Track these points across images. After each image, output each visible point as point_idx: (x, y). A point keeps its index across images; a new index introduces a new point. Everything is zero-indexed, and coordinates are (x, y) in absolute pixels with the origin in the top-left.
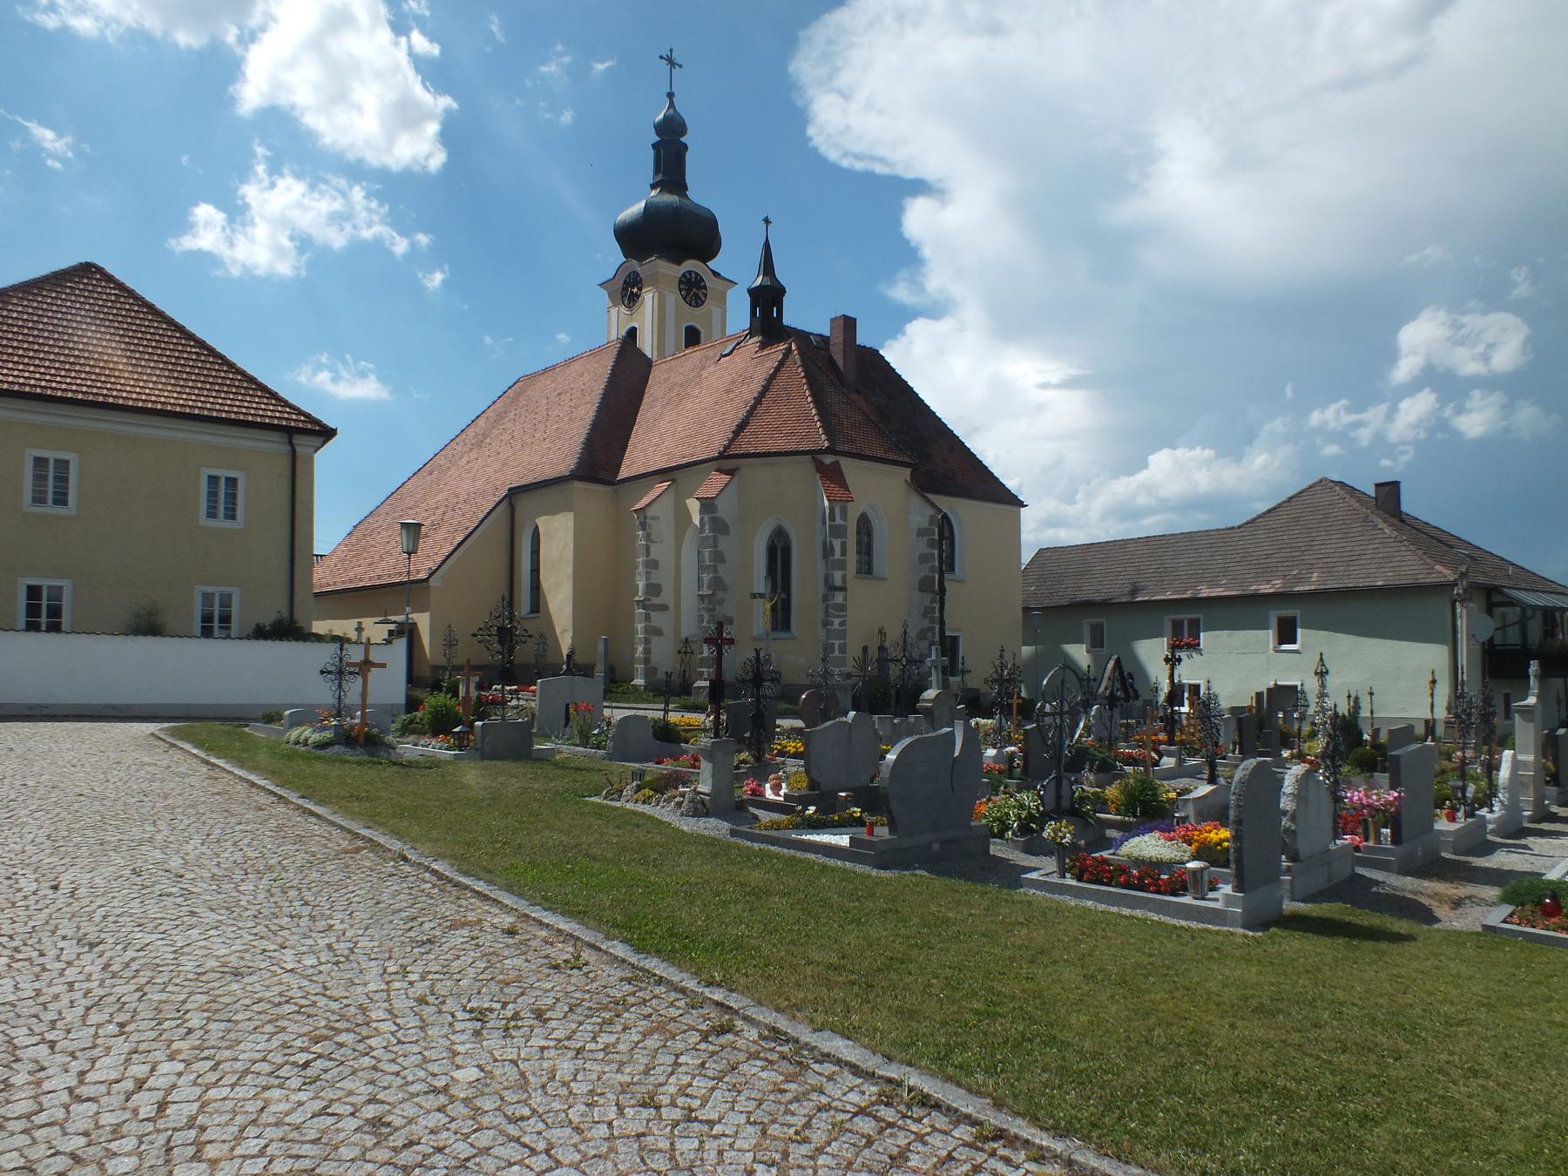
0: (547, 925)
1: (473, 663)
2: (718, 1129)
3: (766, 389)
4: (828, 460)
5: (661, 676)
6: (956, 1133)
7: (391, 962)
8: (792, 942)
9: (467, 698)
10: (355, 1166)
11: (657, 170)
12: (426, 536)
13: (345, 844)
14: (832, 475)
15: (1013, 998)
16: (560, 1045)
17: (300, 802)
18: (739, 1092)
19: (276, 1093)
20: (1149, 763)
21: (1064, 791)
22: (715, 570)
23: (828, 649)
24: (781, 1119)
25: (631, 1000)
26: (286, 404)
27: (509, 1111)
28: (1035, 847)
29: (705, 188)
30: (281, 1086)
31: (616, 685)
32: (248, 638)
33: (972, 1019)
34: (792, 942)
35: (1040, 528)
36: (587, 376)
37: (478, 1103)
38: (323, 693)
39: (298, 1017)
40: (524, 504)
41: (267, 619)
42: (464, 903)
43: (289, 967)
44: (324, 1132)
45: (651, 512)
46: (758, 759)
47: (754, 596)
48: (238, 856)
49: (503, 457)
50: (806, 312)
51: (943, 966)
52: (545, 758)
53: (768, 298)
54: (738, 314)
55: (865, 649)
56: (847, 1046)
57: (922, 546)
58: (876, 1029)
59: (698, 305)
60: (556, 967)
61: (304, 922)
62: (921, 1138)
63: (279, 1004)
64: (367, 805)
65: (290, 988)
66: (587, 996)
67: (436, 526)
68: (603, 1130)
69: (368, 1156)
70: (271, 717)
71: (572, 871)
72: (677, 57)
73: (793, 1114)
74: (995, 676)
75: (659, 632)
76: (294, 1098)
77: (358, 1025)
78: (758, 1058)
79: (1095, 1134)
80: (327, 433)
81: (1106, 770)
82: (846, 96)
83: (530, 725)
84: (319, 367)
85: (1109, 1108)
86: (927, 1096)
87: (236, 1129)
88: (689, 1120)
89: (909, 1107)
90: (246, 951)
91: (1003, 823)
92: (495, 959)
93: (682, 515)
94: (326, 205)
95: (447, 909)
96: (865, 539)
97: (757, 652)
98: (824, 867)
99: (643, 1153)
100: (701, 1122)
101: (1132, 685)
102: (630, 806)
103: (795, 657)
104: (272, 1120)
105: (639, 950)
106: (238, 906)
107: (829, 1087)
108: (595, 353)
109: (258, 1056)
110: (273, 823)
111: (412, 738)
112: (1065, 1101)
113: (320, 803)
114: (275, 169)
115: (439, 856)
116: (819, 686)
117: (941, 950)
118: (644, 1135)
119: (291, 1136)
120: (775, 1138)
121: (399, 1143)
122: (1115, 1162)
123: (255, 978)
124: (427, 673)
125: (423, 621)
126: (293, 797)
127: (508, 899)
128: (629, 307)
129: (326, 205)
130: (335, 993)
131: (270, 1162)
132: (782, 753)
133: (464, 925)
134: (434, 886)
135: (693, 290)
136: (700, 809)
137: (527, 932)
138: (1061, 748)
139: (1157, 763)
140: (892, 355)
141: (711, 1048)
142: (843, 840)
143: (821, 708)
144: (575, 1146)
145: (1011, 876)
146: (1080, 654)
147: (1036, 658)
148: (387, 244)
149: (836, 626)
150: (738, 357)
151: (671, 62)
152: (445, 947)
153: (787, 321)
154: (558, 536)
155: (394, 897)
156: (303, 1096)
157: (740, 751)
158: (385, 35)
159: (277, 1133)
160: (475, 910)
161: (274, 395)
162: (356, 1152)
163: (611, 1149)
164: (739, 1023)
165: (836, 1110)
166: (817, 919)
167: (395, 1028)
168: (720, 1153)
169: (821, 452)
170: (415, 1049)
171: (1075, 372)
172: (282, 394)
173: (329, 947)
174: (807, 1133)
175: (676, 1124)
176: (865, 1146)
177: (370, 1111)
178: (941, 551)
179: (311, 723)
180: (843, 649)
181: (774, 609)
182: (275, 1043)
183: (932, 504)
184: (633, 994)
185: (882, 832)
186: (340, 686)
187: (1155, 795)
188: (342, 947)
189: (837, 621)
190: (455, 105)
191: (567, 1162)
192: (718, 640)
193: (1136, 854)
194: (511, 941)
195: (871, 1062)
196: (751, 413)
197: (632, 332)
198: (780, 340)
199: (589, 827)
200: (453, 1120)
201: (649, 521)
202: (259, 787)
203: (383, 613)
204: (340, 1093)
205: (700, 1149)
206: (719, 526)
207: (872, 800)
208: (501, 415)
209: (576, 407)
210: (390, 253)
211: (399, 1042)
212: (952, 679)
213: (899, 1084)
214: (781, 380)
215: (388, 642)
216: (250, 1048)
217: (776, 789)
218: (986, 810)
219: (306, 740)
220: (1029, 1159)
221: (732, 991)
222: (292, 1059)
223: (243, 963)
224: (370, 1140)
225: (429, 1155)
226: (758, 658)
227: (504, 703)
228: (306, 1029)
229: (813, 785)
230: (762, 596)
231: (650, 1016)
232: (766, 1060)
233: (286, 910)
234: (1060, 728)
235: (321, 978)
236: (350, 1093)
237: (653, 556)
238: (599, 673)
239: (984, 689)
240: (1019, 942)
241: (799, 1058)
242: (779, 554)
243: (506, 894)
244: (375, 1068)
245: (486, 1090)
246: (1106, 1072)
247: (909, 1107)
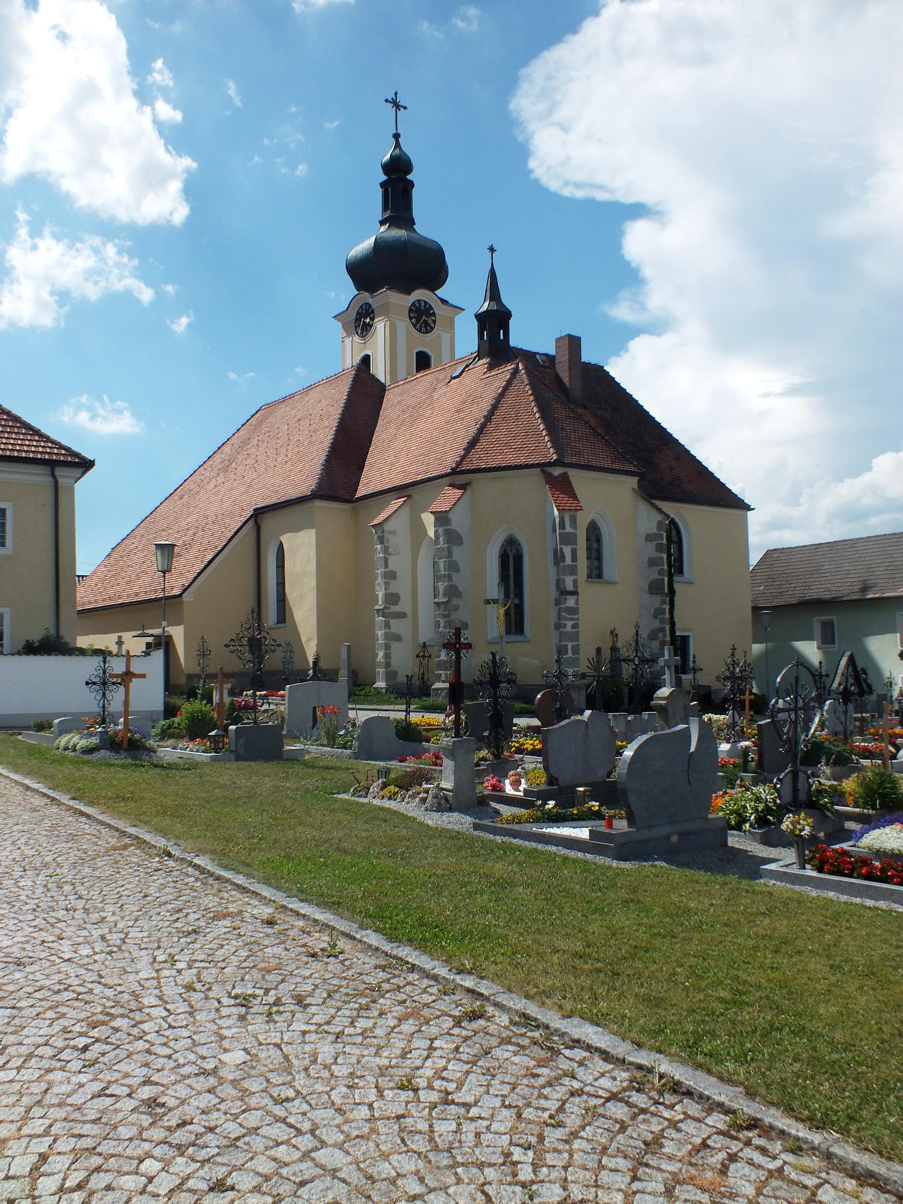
0: (304, 916)
1: (226, 670)
2: (474, 1112)
3: (495, 407)
4: (557, 471)
5: (401, 678)
6: (710, 1121)
7: (161, 951)
8: (538, 931)
9: (221, 703)
10: (133, 1145)
11: (385, 208)
12: (179, 555)
13: (113, 841)
14: (562, 486)
15: (759, 987)
16: (320, 1029)
17: (71, 803)
18: (493, 1076)
19: (58, 1076)
20: (887, 756)
21: (801, 785)
22: (450, 578)
23: (561, 650)
24: (535, 1103)
25: (386, 986)
26: (48, 439)
27: (275, 1092)
28: (773, 838)
29: (429, 221)
30: (62, 1069)
31: (359, 688)
32: (19, 653)
33: (719, 1008)
34: (538, 931)
35: (764, 533)
36: (324, 403)
37: (246, 1084)
38: (89, 702)
39: (76, 1004)
40: (269, 523)
41: (36, 636)
42: (225, 895)
43: (66, 956)
44: (103, 1112)
45: (388, 527)
46: (497, 756)
47: (488, 602)
48: (17, 854)
49: (247, 480)
50: (530, 334)
51: (686, 955)
52: (295, 758)
53: (494, 322)
54: (466, 337)
55: (599, 650)
56: (596, 1033)
57: (650, 550)
58: (624, 1016)
59: (427, 332)
60: (314, 955)
61: (79, 914)
62: (674, 1125)
63: (59, 991)
64: (132, 804)
65: (68, 976)
66: (344, 983)
67: (187, 546)
68: (364, 1112)
69: (145, 1135)
70: (42, 726)
71: (325, 864)
72: (402, 100)
73: (546, 1098)
74: (727, 674)
75: (398, 638)
76: (75, 1079)
77: (131, 1011)
78: (510, 1043)
79: (853, 1127)
80: (86, 465)
81: (843, 763)
82: (565, 128)
83: (280, 727)
84: (79, 408)
85: (865, 1101)
86: (678, 1083)
87: (23, 1109)
88: (447, 1102)
89: (661, 1093)
90: (27, 942)
91: (740, 815)
92: (255, 948)
93: (418, 528)
94: (84, 262)
95: (210, 901)
96: (595, 545)
97: (494, 655)
98: (565, 859)
99: (404, 1135)
100: (458, 1104)
101: (865, 680)
102: (376, 802)
103: (529, 659)
104: (55, 1101)
105: (391, 939)
106: (18, 900)
107: (580, 1072)
108: (331, 380)
109: (42, 1040)
110: (47, 823)
111: (171, 742)
112: (818, 1091)
113: (90, 803)
114: (36, 232)
115: (200, 852)
116: (554, 686)
117: (684, 939)
118: (403, 1116)
119: (72, 1117)
120: (530, 1122)
121: (173, 1123)
122: (876, 1157)
123: (35, 967)
124: (182, 681)
125: (177, 633)
126: (65, 799)
127: (266, 892)
128: (363, 336)
129: (84, 262)
130: (110, 981)
131: (55, 1141)
132: (520, 751)
133: (225, 916)
134: (197, 880)
135: (423, 318)
136: (444, 804)
137: (285, 922)
138: (797, 743)
139: (894, 757)
140: (617, 370)
141: (464, 1033)
142: (582, 833)
143: (555, 709)
144: (338, 1126)
145: (751, 867)
146: (810, 651)
147: (766, 654)
148: (135, 293)
149: (569, 628)
150: (467, 378)
151: (397, 105)
152: (209, 937)
153: (512, 343)
154: (301, 552)
155: (160, 890)
156: (83, 1078)
157: (479, 749)
158: (133, 103)
159: (60, 1113)
160: (236, 902)
161: (37, 432)
162: (133, 1131)
163: (373, 1130)
164: (490, 1010)
165: (589, 1095)
166: (561, 909)
167: (165, 1014)
168: (478, 1135)
169: (550, 464)
170: (185, 1033)
171: (797, 380)
172: (44, 431)
173: (103, 938)
174: (561, 1117)
175: (433, 1106)
176: (619, 1132)
177: (146, 1092)
178: (669, 556)
179: (78, 730)
180: (576, 650)
181: (507, 613)
182: (56, 1028)
183: (659, 510)
184: (388, 981)
185: (621, 825)
186: (104, 695)
187: (894, 788)
188: (114, 938)
189: (569, 624)
190: (194, 165)
191: (331, 1142)
192: (456, 645)
193: (877, 845)
194: (270, 931)
195: (621, 1048)
196: (481, 430)
197: (366, 360)
198: (507, 361)
199: (339, 823)
200: (223, 1101)
201: (386, 535)
202: (34, 790)
203: (141, 628)
204: (117, 1075)
205: (458, 1131)
206: (453, 538)
207: (611, 794)
208: (246, 442)
209: (315, 431)
210: (138, 301)
211: (170, 1027)
212: (684, 677)
213: (650, 1070)
214: (509, 398)
215: (147, 654)
216: (33, 1033)
217: (516, 784)
218: (723, 803)
219: (75, 746)
220: (786, 1150)
221: (482, 978)
222: (72, 1043)
223: (24, 954)
224: (146, 1120)
225: (202, 1135)
226: (494, 661)
227: (254, 708)
228: (84, 1015)
229: (551, 780)
230: (495, 601)
231: (404, 1002)
232: (518, 1045)
233: (63, 904)
234: (795, 723)
235: (96, 967)
236: (127, 1075)
237: (391, 567)
238: (343, 677)
239: (715, 685)
240: (762, 932)
241: (551, 1045)
242: (511, 561)
243: (264, 887)
244: (148, 1051)
245: (253, 1072)
246: (859, 1064)
247: (661, 1093)
